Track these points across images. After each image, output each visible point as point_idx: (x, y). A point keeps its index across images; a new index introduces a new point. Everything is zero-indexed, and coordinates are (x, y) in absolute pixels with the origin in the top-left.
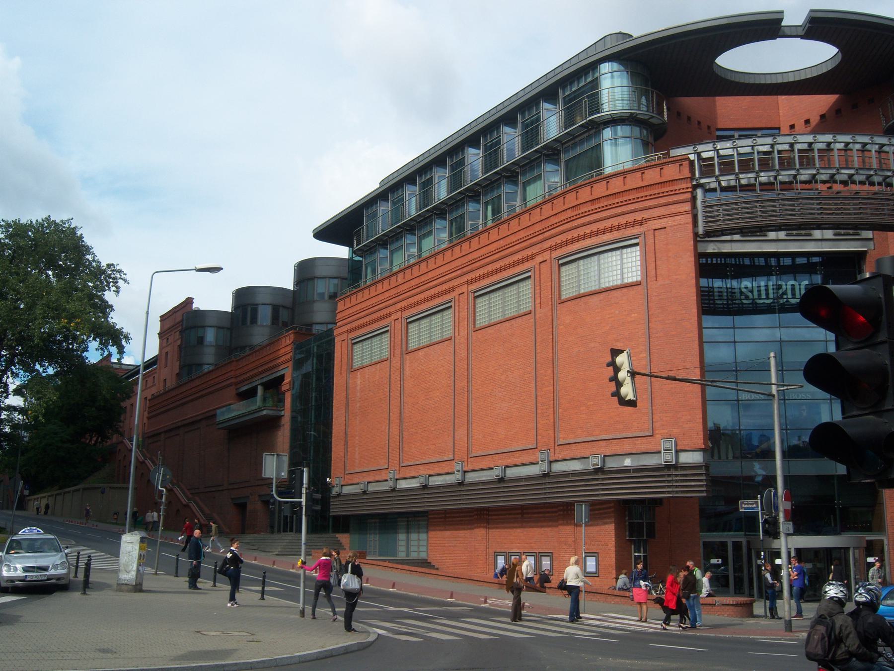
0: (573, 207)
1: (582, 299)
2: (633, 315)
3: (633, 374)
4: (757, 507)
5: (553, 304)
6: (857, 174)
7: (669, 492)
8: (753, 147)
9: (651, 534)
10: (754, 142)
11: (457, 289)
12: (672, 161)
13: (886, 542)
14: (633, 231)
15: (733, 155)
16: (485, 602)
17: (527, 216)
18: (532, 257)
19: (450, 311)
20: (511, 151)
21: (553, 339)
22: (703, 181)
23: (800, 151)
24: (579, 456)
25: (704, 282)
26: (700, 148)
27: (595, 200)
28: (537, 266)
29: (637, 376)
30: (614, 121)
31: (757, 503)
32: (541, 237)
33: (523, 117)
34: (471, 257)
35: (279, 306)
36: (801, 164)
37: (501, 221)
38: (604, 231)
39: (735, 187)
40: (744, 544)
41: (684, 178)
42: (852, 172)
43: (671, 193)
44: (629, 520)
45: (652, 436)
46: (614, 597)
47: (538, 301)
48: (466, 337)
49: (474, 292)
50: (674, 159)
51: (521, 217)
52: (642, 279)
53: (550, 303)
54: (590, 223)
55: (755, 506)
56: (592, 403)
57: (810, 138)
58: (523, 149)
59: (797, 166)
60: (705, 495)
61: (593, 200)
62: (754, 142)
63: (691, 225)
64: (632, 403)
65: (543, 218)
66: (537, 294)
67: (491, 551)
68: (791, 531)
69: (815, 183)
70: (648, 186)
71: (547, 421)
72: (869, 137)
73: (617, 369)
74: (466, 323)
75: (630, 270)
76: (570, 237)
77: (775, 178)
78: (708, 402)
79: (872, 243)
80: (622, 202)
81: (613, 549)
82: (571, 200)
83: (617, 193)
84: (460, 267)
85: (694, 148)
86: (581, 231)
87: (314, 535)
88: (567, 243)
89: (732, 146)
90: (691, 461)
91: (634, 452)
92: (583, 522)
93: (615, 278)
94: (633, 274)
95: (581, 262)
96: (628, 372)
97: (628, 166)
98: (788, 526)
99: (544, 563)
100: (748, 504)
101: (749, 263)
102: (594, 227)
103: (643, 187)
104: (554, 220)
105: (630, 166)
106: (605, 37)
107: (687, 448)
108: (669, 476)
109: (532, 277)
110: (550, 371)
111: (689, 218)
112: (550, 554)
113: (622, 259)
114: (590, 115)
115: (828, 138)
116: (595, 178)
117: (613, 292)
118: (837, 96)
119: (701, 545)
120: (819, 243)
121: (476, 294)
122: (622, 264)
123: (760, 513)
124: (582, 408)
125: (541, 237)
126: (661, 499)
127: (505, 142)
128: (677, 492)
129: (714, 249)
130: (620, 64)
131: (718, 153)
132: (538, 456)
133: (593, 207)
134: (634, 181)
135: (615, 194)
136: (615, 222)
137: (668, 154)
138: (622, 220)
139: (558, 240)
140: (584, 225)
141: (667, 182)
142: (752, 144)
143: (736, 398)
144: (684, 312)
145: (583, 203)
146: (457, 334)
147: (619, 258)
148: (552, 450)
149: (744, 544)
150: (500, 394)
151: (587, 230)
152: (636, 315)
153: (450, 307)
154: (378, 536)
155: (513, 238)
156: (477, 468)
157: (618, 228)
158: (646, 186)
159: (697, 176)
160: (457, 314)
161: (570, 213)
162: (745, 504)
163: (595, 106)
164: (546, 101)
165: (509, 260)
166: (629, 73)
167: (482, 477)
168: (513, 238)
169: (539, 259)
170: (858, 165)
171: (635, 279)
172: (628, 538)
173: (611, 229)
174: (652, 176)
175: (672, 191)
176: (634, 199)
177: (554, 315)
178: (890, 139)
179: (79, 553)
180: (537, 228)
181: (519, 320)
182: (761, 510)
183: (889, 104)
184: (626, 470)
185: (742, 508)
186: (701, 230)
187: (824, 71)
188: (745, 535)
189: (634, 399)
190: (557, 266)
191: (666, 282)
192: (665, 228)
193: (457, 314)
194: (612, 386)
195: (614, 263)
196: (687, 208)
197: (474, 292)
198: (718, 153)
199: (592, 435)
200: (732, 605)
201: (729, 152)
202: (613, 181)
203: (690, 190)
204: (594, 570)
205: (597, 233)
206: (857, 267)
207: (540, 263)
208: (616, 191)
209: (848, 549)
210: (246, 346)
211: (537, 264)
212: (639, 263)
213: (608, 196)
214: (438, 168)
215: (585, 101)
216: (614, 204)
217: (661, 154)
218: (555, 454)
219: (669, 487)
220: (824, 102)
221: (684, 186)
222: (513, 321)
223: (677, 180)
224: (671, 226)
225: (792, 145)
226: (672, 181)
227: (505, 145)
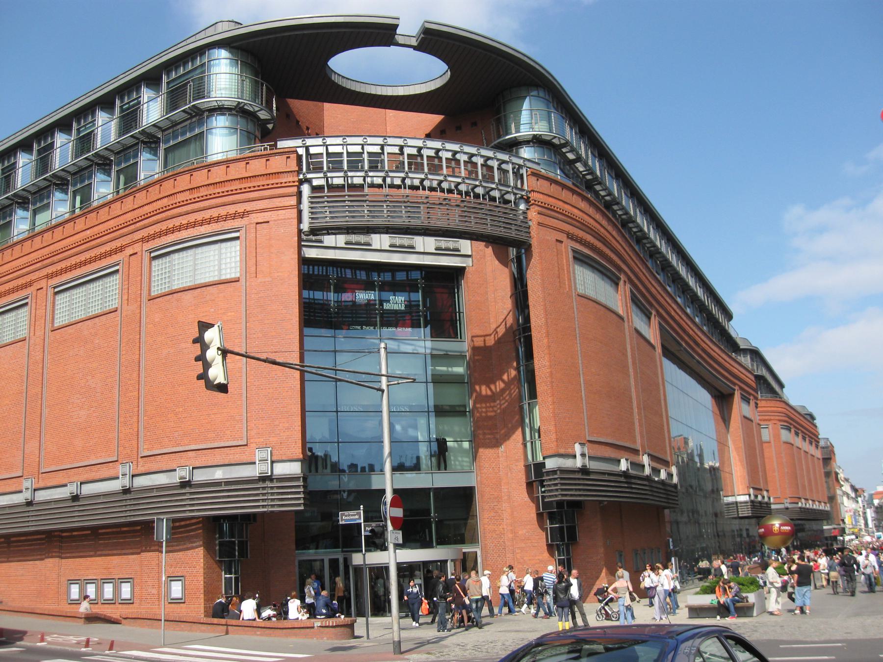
0: (169, 196)
1: (175, 295)
2: (230, 314)
3: (224, 352)
4: (360, 518)
5: (142, 300)
6: (464, 182)
7: (263, 506)
8: (363, 145)
9: (243, 553)
10: (365, 140)
11: (35, 284)
12: (279, 153)
13: (479, 554)
14: (233, 224)
15: (343, 153)
16: (42, 640)
17: (118, 204)
18: (121, 249)
19: (25, 310)
20: (106, 135)
21: (140, 339)
22: (309, 176)
23: (409, 156)
25: (305, 294)
26: (309, 142)
27: (194, 188)
28: (126, 259)
29: (229, 355)
30: (220, 110)
33: (122, 101)
34: (52, 248)
36: (410, 168)
37: (90, 209)
38: (202, 223)
39: (343, 186)
40: (341, 561)
41: (291, 172)
42: (459, 180)
43: (276, 186)
44: (220, 538)
45: (246, 445)
47: (125, 297)
48: (42, 338)
49: (54, 288)
50: (282, 151)
51: (112, 206)
52: (241, 275)
53: (139, 300)
55: (357, 517)
56: (181, 409)
57: (420, 143)
58: (120, 133)
59: (406, 169)
60: (303, 508)
61: (192, 189)
62: (365, 140)
63: (296, 220)
64: (223, 388)
65: (136, 207)
67: (63, 580)
68: (401, 541)
69: (422, 189)
70: (253, 177)
72: (476, 149)
73: (205, 347)
74: (43, 321)
75: (228, 265)
76: (164, 228)
77: (384, 180)
78: (307, 413)
79: (470, 259)
80: (223, 192)
81: (202, 571)
82: (168, 187)
83: (219, 183)
84: (40, 259)
85: (302, 141)
86: (177, 222)
88: (160, 234)
89: (342, 143)
92: (164, 539)
93: (212, 274)
94: (231, 270)
95: (176, 256)
96: (218, 348)
97: (232, 155)
98: (397, 535)
100: (349, 515)
101: (351, 277)
103: (247, 178)
104: (147, 209)
105: (233, 156)
106: (216, 23)
107: (284, 458)
108: (264, 488)
109: (121, 272)
110: (135, 375)
111: (294, 212)
113: (220, 254)
114: (194, 100)
115: (437, 144)
116: (196, 165)
118: (442, 117)
119: (297, 564)
120: (421, 256)
121: (56, 290)
122: (220, 260)
124: (169, 416)
126: (254, 515)
127: (100, 124)
128: (273, 506)
129: (317, 255)
130: (230, 52)
131: (327, 149)
132: (121, 470)
134: (237, 170)
135: (216, 183)
136: (214, 213)
137: (276, 145)
138: (223, 211)
139: (151, 230)
141: (272, 174)
142: (363, 143)
143: (335, 410)
144: (285, 311)
145: (180, 192)
146: (32, 334)
147: (217, 252)
148: (135, 463)
149: (341, 561)
150: (79, 401)
153: (26, 304)
154: (561, 629)
155: (102, 228)
156: (49, 485)
157: (217, 219)
158: (250, 177)
159: (304, 170)
160: (33, 311)
161: (165, 202)
162: (346, 516)
163: (200, 93)
166: (239, 62)
168: (102, 228)
169: (129, 251)
170: (465, 174)
171: (233, 276)
172: (218, 559)
173: (210, 221)
174: (257, 166)
175: (277, 184)
176: (236, 190)
177: (142, 312)
178: (495, 153)
180: (129, 216)
182: (364, 522)
183: (492, 127)
186: (305, 226)
187: (433, 88)
188: (343, 552)
189: (225, 382)
190: (148, 260)
191: (267, 279)
192: (268, 222)
193: (33, 311)
194: (199, 367)
195: (212, 258)
196: (292, 202)
197: (54, 288)
198: (327, 149)
199: (178, 445)
200: (332, 627)
201: (338, 149)
202: (214, 170)
203: (297, 184)
204: (179, 595)
205: (194, 224)
206: (456, 283)
207: (131, 255)
208: (218, 180)
209: (446, 561)
211: (126, 256)
212: (238, 259)
213: (208, 185)
214: (23, 153)
215: (190, 85)
216: (214, 194)
217: (267, 145)
218: (137, 467)
219: (263, 500)
220: (433, 120)
221: (291, 179)
222: (97, 319)
223: (283, 172)
224: (275, 220)
227: (100, 129)
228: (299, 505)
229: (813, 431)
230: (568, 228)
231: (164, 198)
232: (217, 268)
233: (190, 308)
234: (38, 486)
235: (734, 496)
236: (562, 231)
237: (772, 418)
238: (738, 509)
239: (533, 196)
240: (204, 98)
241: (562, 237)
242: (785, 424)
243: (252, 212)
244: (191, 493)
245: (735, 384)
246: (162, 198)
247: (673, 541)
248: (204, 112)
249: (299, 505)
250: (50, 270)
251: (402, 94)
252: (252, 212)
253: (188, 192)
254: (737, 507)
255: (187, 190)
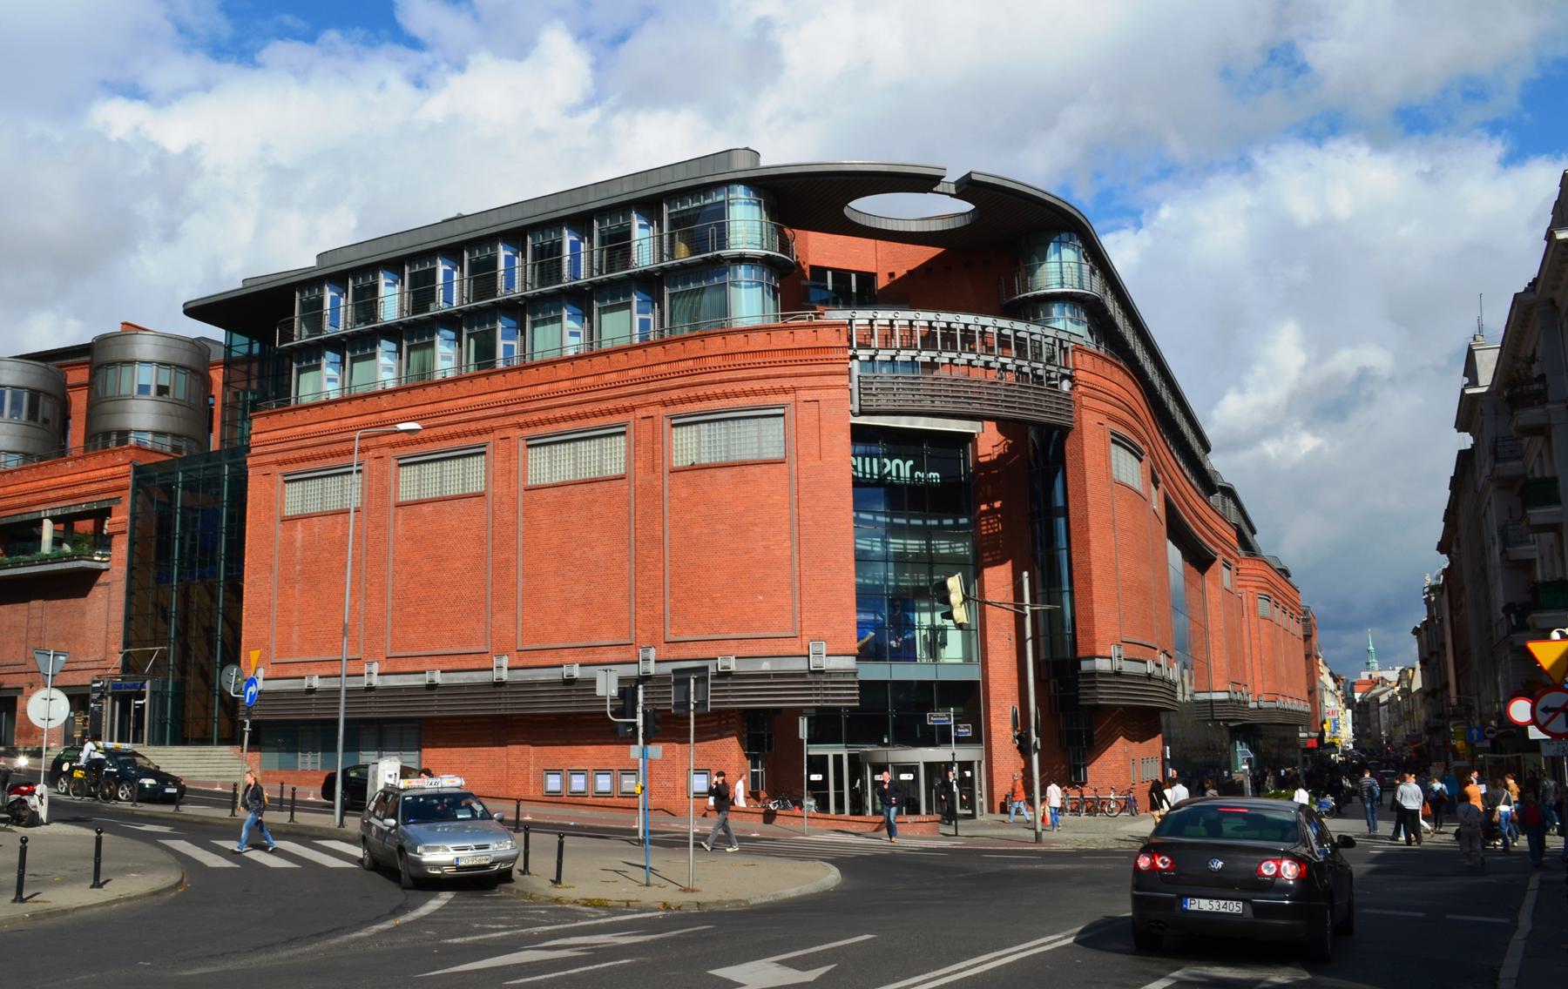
1: (707, 471)
2: (775, 497)
4: (950, 720)
7: (817, 701)
14: (777, 399)
24: (700, 657)
30: (741, 259)
31: (949, 716)
32: (643, 388)
35: (39, 391)
36: (963, 348)
46: (793, 818)
54: (721, 382)
55: (947, 719)
59: (959, 349)
61: (725, 355)
66: (632, 456)
71: (652, 613)
87: (348, 754)
90: (842, 667)
91: (775, 654)
97: (757, 322)
99: (626, 782)
102: (728, 388)
107: (839, 652)
112: (708, 772)
117: (752, 467)
123: (953, 727)
125: (643, 388)
128: (826, 701)
133: (725, 363)
134: (758, 341)
138: (766, 384)
140: (713, 383)
141: (821, 348)
151: (718, 389)
152: (779, 497)
159: (855, 346)
163: (722, 241)
164: (641, 213)
165: (591, 408)
167: (540, 676)
169: (641, 413)
174: (782, 340)
179: (294, 789)
181: (606, 485)
184: (765, 675)
185: (930, 720)
188: (847, 747)
199: (715, 632)
210: (855, 548)
215: (713, 230)
216: (754, 363)
222: (595, 485)
224: (825, 400)
225: (891, 321)
226: (827, 347)
228: (854, 701)
229: (1296, 600)
230: (1109, 408)
231: (688, 359)
232: (756, 445)
233: (727, 487)
234: (514, 665)
235: (1208, 692)
236: (1103, 412)
237: (1248, 583)
238: (1212, 710)
239: (1080, 374)
240: (725, 249)
241: (1103, 419)
242: (1265, 593)
243: (800, 388)
244: (733, 684)
245: (1217, 546)
246: (686, 360)
247: (1170, 750)
248: (725, 260)
249: (854, 701)
250: (521, 419)
251: (915, 230)
252: (800, 388)
253: (720, 358)
254: (1212, 706)
255: (719, 355)
